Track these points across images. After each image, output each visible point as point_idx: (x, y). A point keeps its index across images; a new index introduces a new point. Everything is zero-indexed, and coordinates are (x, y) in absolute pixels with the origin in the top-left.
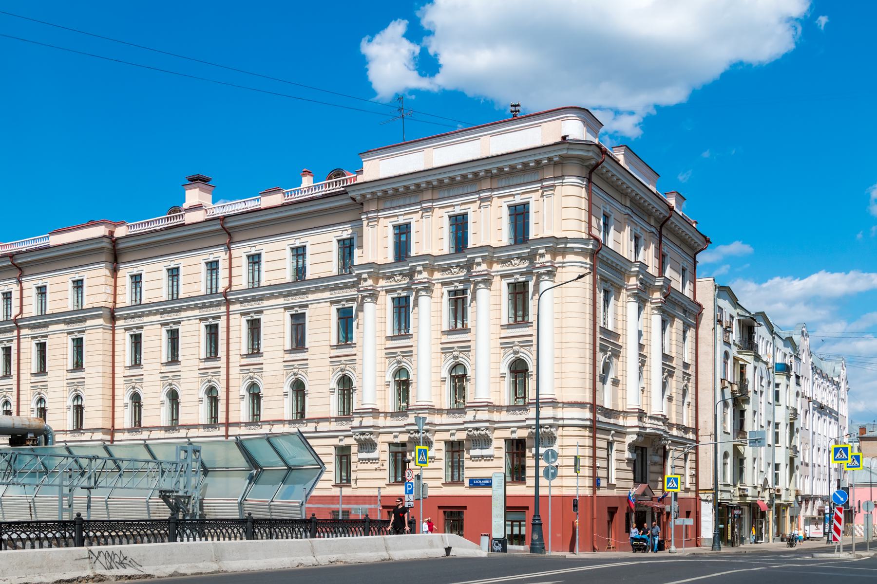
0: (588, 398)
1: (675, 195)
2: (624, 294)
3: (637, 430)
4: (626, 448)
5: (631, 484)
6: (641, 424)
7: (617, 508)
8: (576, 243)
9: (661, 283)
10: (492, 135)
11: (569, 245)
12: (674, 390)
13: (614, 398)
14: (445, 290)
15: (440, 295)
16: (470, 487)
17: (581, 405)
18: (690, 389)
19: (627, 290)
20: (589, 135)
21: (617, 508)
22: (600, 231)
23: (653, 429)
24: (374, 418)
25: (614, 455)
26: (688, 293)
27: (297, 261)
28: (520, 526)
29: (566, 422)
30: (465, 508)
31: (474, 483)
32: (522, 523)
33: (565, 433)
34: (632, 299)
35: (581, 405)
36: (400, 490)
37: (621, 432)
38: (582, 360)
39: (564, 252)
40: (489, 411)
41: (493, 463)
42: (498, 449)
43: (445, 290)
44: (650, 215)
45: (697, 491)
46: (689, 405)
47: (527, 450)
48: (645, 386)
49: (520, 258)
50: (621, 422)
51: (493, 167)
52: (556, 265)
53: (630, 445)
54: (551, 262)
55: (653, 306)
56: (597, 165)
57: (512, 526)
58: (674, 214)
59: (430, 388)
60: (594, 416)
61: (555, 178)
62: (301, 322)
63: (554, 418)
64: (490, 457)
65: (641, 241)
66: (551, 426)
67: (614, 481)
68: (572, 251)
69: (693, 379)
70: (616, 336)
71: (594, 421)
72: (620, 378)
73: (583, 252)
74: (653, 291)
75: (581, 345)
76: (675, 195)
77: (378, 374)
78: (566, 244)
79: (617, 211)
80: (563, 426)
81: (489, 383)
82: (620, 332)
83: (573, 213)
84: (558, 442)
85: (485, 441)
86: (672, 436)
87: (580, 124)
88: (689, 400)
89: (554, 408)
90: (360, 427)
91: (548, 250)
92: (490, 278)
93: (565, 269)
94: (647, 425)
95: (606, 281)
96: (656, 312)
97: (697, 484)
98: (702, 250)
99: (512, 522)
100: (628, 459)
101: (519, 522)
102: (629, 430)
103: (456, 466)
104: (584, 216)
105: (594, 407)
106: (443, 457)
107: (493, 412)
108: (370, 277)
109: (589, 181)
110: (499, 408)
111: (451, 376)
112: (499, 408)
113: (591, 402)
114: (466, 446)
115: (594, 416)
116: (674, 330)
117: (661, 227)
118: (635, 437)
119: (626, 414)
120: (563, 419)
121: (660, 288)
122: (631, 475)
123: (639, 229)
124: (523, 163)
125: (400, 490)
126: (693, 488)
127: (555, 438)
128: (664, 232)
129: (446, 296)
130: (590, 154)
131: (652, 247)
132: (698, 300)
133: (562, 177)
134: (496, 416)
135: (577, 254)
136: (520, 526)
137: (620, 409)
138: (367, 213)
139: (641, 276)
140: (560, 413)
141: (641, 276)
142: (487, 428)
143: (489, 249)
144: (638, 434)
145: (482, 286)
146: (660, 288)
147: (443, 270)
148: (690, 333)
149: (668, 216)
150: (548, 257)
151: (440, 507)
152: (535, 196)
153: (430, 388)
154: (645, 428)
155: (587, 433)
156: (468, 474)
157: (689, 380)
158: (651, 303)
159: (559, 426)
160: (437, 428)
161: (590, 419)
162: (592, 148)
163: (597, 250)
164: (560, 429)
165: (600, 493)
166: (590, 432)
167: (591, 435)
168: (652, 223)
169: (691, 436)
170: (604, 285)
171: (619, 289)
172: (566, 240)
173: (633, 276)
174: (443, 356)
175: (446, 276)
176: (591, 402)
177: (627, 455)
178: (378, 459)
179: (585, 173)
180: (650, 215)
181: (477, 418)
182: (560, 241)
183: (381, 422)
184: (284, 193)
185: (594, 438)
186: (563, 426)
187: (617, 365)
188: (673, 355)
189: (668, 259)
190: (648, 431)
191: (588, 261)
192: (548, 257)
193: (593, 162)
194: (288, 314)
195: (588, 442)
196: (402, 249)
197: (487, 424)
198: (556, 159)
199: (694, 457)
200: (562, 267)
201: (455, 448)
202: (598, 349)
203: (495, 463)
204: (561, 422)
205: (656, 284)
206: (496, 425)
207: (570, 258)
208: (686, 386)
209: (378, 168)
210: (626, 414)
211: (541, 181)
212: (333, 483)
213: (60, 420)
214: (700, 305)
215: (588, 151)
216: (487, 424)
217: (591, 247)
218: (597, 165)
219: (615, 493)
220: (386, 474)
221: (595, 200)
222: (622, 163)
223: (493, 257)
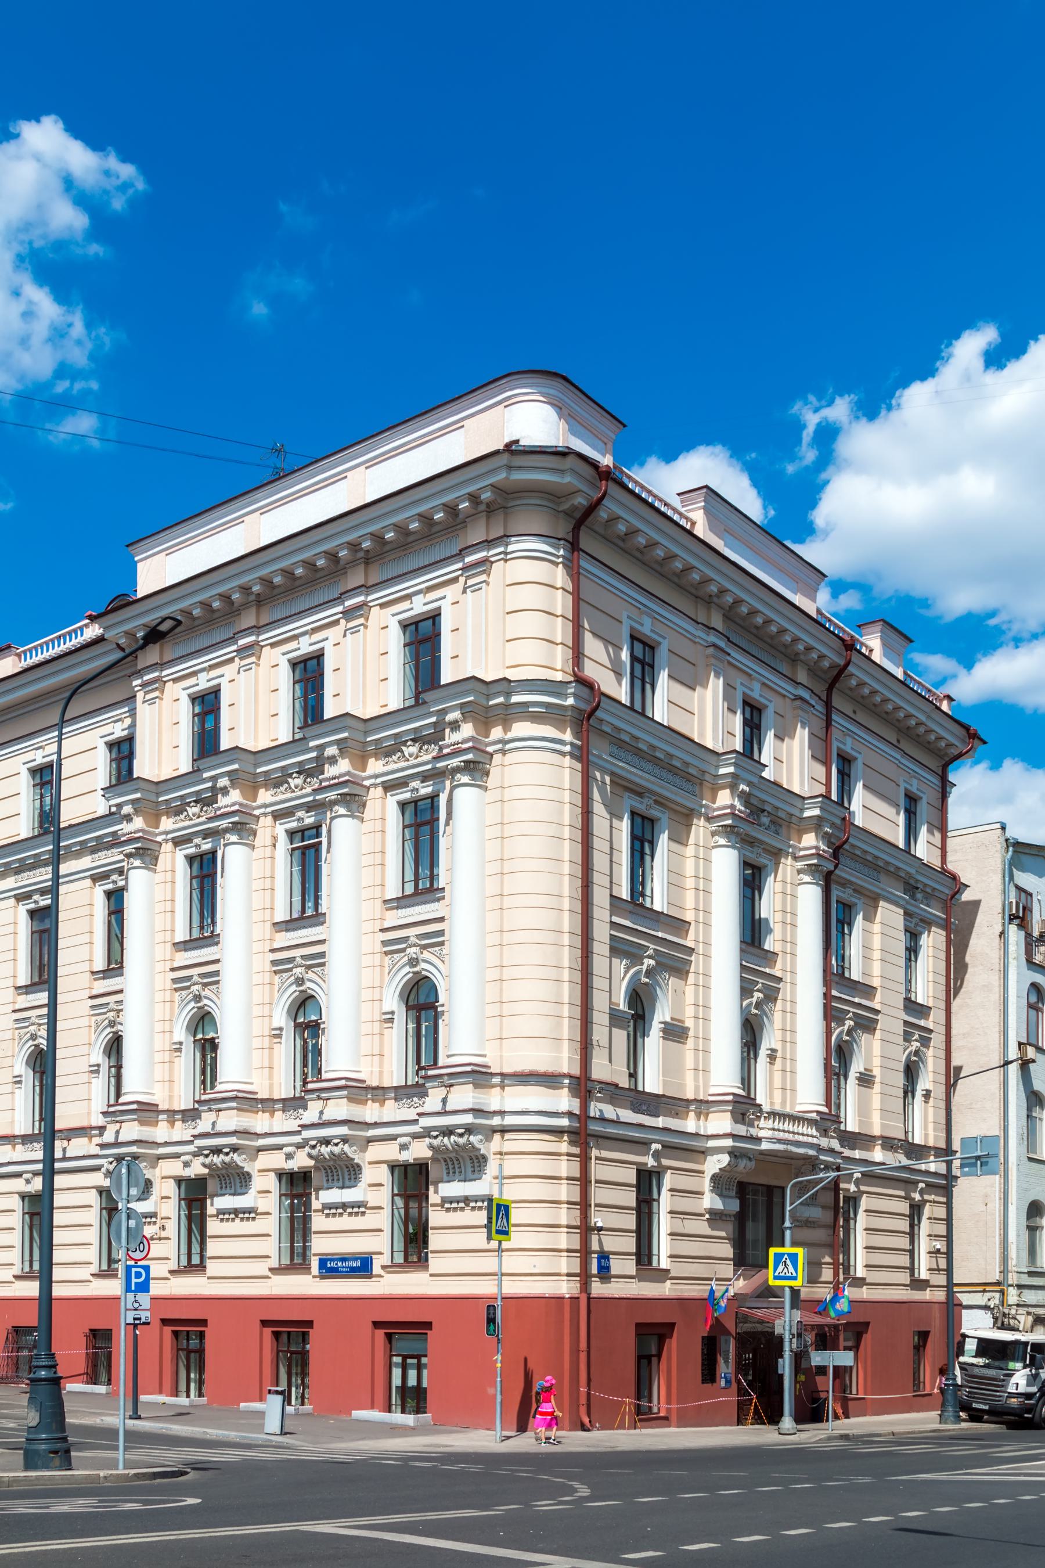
0: (566, 1061)
1: (878, 627)
2: (700, 829)
3: (729, 1142)
4: (706, 1185)
5: (727, 1270)
6: (742, 1130)
7: (672, 1325)
8: (531, 692)
9: (816, 812)
10: (370, 464)
11: (515, 699)
12: (877, 1062)
13: (671, 1068)
14: (281, 830)
15: (269, 841)
16: (322, 1277)
17: (549, 1080)
18: (930, 1061)
19: (709, 819)
20: (574, 433)
21: (672, 1325)
22: (619, 675)
23: (780, 1141)
24: (142, 1123)
25: (925, 1227)
26: (924, 848)
27: (42, 797)
28: (419, 1368)
29: (510, 1120)
30: (310, 1324)
31: (330, 1268)
32: (424, 1360)
33: (508, 1146)
34: (722, 841)
35: (549, 1080)
36: (113, 1287)
37: (689, 1149)
38: (552, 973)
39: (508, 715)
40: (350, 1099)
41: (360, 1221)
42: (375, 1188)
43: (281, 830)
44: (794, 659)
45: (950, 1285)
46: (927, 1095)
47: (431, 1189)
48: (778, 1046)
49: (419, 739)
50: (690, 1124)
51: (362, 534)
52: (490, 749)
53: (715, 1178)
54: (472, 739)
55: (799, 865)
56: (593, 507)
57: (404, 1368)
58: (855, 658)
59: (254, 1059)
60: (585, 1107)
61: (489, 543)
62: (47, 924)
63: (477, 1112)
64: (358, 1208)
65: (768, 717)
66: (469, 1130)
67: (924, 1275)
68: (523, 712)
69: (938, 1040)
70: (680, 925)
71: (583, 1117)
72: (689, 1023)
73: (550, 715)
74: (801, 833)
75: (550, 937)
76: (878, 627)
77: (158, 1027)
78: (508, 694)
79: (672, 632)
80: (503, 1130)
81: (362, 1041)
82: (689, 916)
83: (532, 624)
84: (492, 1167)
85: (345, 1172)
86: (927, 1173)
87: (547, 412)
88: (929, 1086)
89: (477, 1086)
90: (116, 1144)
91: (468, 712)
92: (357, 790)
93: (510, 758)
94: (762, 1134)
95: (640, 795)
96: (807, 878)
97: (949, 1271)
98: (960, 755)
99: (405, 1358)
100: (712, 1212)
101: (418, 1357)
102: (711, 1144)
103: (298, 1228)
104: (561, 631)
105: (583, 1086)
106: (274, 1209)
107: (364, 1102)
108: (137, 812)
109: (574, 546)
110: (378, 1093)
111: (297, 1026)
112: (378, 1093)
113: (576, 1071)
114: (315, 1182)
115: (585, 1107)
116: (876, 928)
117: (830, 690)
118: (725, 1159)
119: (703, 1106)
120: (502, 1113)
121: (817, 824)
122: (727, 1250)
123: (757, 686)
124: (421, 516)
125: (113, 1287)
126: (941, 1279)
127: (484, 1158)
128: (837, 701)
129: (283, 845)
130: (568, 479)
131: (802, 735)
132: (950, 866)
133: (504, 539)
134: (370, 1112)
135: (536, 718)
136: (419, 1368)
137: (690, 1095)
138: (139, 673)
139: (743, 787)
140: (493, 1099)
141: (743, 787)
142: (345, 1140)
143: (350, 722)
144: (733, 1153)
145: (342, 811)
146: (817, 824)
147: (278, 781)
148: (932, 942)
149: (842, 663)
150: (467, 730)
151: (265, 1323)
152: (451, 592)
153: (254, 1059)
154: (758, 1140)
155: (564, 1147)
156: (319, 1245)
157: (925, 1042)
158: (796, 858)
159: (494, 1130)
160: (262, 1142)
161: (570, 1114)
162: (570, 461)
163: (588, 708)
164: (497, 1137)
165: (598, 1289)
166: (572, 1143)
167: (576, 1150)
168: (802, 676)
169: (934, 1166)
170: (629, 801)
171: (685, 818)
172: (505, 685)
173: (723, 788)
174: (277, 979)
175: (281, 797)
176: (576, 1071)
177: (710, 1201)
178: (154, 1215)
179: (564, 529)
180: (794, 659)
181: (325, 1117)
182: (495, 688)
183: (161, 1132)
184: (19, 655)
185: (585, 1160)
186: (503, 1130)
187: (679, 994)
188: (876, 982)
189: (858, 768)
190: (765, 1146)
191: (568, 736)
192: (467, 730)
193: (580, 501)
194: (22, 910)
195: (566, 1167)
196: (206, 743)
197: (344, 1130)
198: (486, 496)
199: (941, 1212)
200: (504, 752)
201: (297, 1185)
202: (601, 948)
203: (369, 1220)
204: (496, 1121)
205: (806, 814)
206: (371, 1133)
207: (522, 728)
208: (917, 1053)
209: (159, 569)
210: (703, 1106)
211: (461, 554)
212: (94, 1269)
213: (99, 1179)
214: (954, 877)
215: (561, 472)
216: (344, 1130)
217: (570, 701)
218: (593, 507)
219: (666, 1289)
220: (272, 1248)
221: (588, 590)
222: (700, 531)
223: (365, 743)
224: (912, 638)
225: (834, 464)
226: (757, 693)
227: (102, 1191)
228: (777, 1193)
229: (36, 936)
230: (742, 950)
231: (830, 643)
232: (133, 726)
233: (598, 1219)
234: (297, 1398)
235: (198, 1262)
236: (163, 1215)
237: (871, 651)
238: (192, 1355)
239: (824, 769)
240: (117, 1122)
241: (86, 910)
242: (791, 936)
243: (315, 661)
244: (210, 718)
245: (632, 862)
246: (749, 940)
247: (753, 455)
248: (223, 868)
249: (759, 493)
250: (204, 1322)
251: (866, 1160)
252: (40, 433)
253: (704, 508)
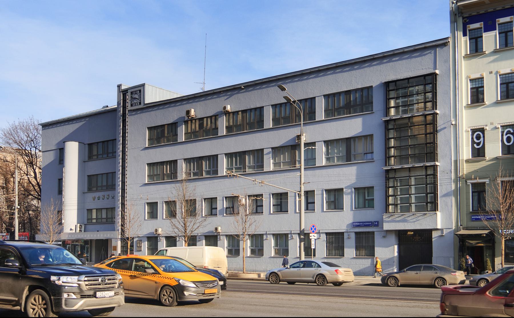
209: (412, 233)
228: (357, 207)
229: (476, 194)
232: (163, 237)
233: (283, 109)
234: (404, 221)
236: (432, 66)
238: (429, 204)
241: (442, 182)
242: (309, 277)
243: (258, 112)
245: (232, 285)
246: (506, 152)
250: (262, 195)
252: (53, 278)
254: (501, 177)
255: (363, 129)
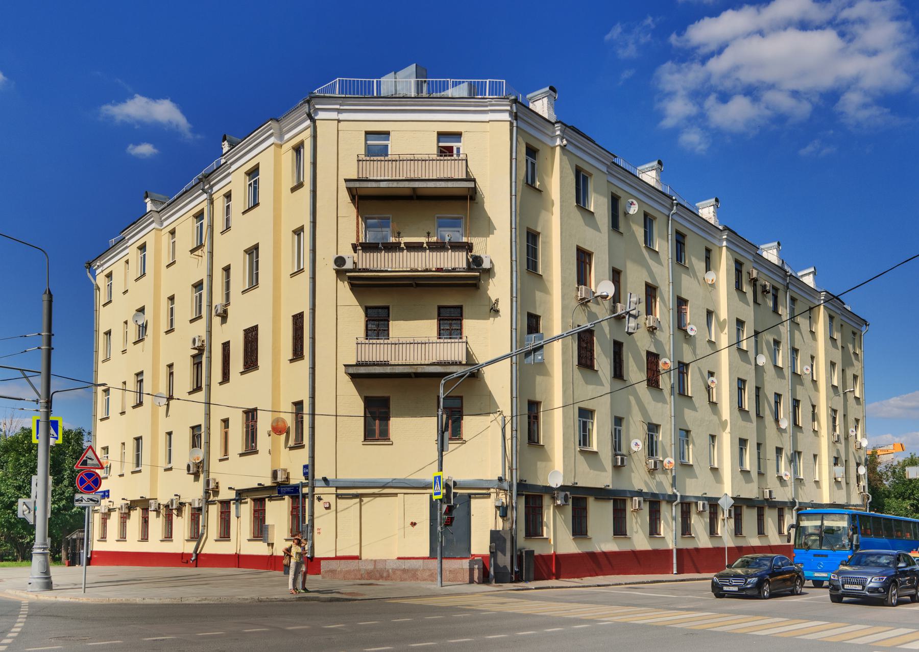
10: (386, 364)
224: (869, 322)
225: (758, 11)
226: (833, 314)
227: (511, 112)
230: (469, 179)
231: (370, 185)
235: (270, 506)
237: (107, 360)
239: (803, 518)
240: (360, 271)
244: (323, 483)
247: (831, 132)
248: (374, 364)
249: (733, 9)
251: (273, 318)
253: (814, 273)
254: (713, 505)
255: (165, 98)
